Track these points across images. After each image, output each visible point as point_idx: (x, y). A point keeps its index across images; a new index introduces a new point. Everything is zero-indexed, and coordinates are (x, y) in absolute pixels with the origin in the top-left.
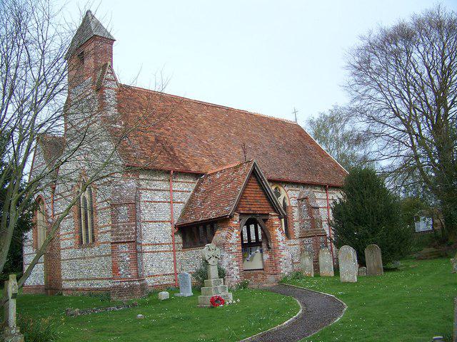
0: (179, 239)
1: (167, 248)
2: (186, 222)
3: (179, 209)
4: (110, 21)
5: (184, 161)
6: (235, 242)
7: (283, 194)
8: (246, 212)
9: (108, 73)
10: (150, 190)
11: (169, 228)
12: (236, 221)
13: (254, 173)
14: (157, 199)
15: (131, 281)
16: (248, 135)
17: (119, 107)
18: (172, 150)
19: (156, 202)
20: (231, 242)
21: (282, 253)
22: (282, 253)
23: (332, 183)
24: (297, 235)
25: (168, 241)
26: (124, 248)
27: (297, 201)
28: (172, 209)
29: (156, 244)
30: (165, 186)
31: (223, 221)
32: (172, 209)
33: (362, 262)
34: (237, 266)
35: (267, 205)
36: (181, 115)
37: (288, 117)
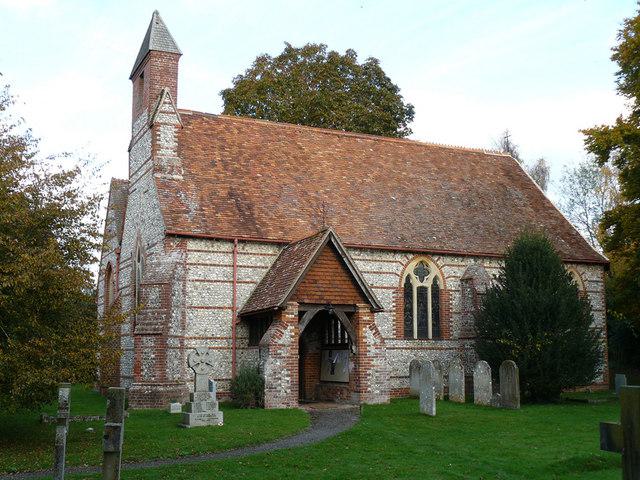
0: (243, 332)
1: (224, 344)
2: (250, 309)
5: (264, 224)
6: (287, 343)
7: (434, 271)
8: (313, 302)
9: (165, 103)
10: (203, 265)
11: (228, 317)
13: (330, 244)
14: (213, 277)
15: (154, 385)
16: (399, 180)
17: (179, 150)
18: (250, 208)
19: (212, 281)
20: (280, 342)
21: (372, 363)
22: (372, 363)
24: (456, 334)
25: (225, 334)
26: (149, 342)
27: (459, 283)
28: (234, 291)
29: (207, 338)
30: (228, 260)
32: (234, 291)
33: (495, 377)
34: (288, 376)
35: (353, 292)
36: (287, 154)
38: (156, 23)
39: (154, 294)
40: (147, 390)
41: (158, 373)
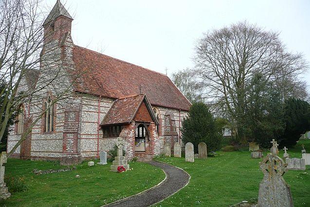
0: (101, 132)
3: (102, 116)
4: (71, 3)
9: (68, 38)
11: (96, 126)
12: (133, 125)
13: (144, 101)
23: (182, 108)
24: (163, 134)
26: (71, 136)
28: (99, 116)
31: (126, 125)
32: (99, 116)
37: (163, 72)
38: (58, 7)
39: (72, 115)
40: (69, 156)
41: (75, 149)
